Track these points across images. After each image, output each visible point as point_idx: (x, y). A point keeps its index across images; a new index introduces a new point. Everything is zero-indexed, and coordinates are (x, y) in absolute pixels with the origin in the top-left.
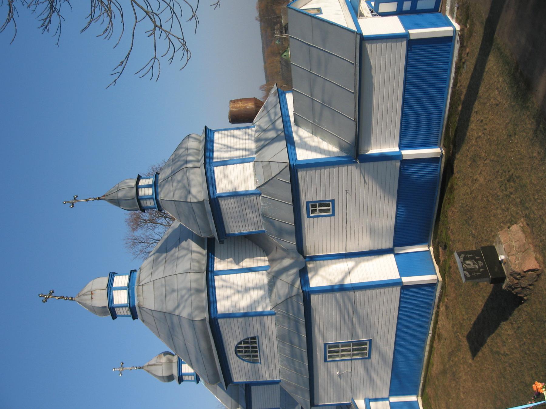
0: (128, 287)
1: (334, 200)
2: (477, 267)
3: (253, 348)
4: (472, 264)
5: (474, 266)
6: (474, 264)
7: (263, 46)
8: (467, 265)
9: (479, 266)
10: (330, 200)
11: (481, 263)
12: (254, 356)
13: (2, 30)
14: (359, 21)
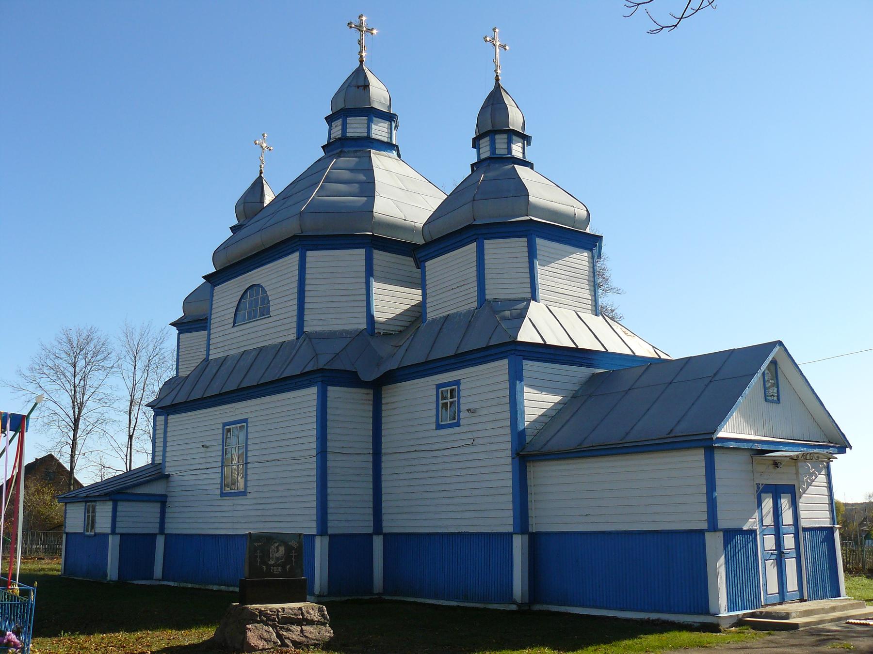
0: (480, 149)
1: (459, 426)
2: (272, 562)
3: (92, 517)
4: (277, 555)
5: (272, 558)
6: (278, 559)
7: (849, 504)
8: (277, 547)
9: (273, 565)
10: (459, 419)
11: (277, 570)
12: (24, 559)
13: (650, 32)
14: (373, 126)
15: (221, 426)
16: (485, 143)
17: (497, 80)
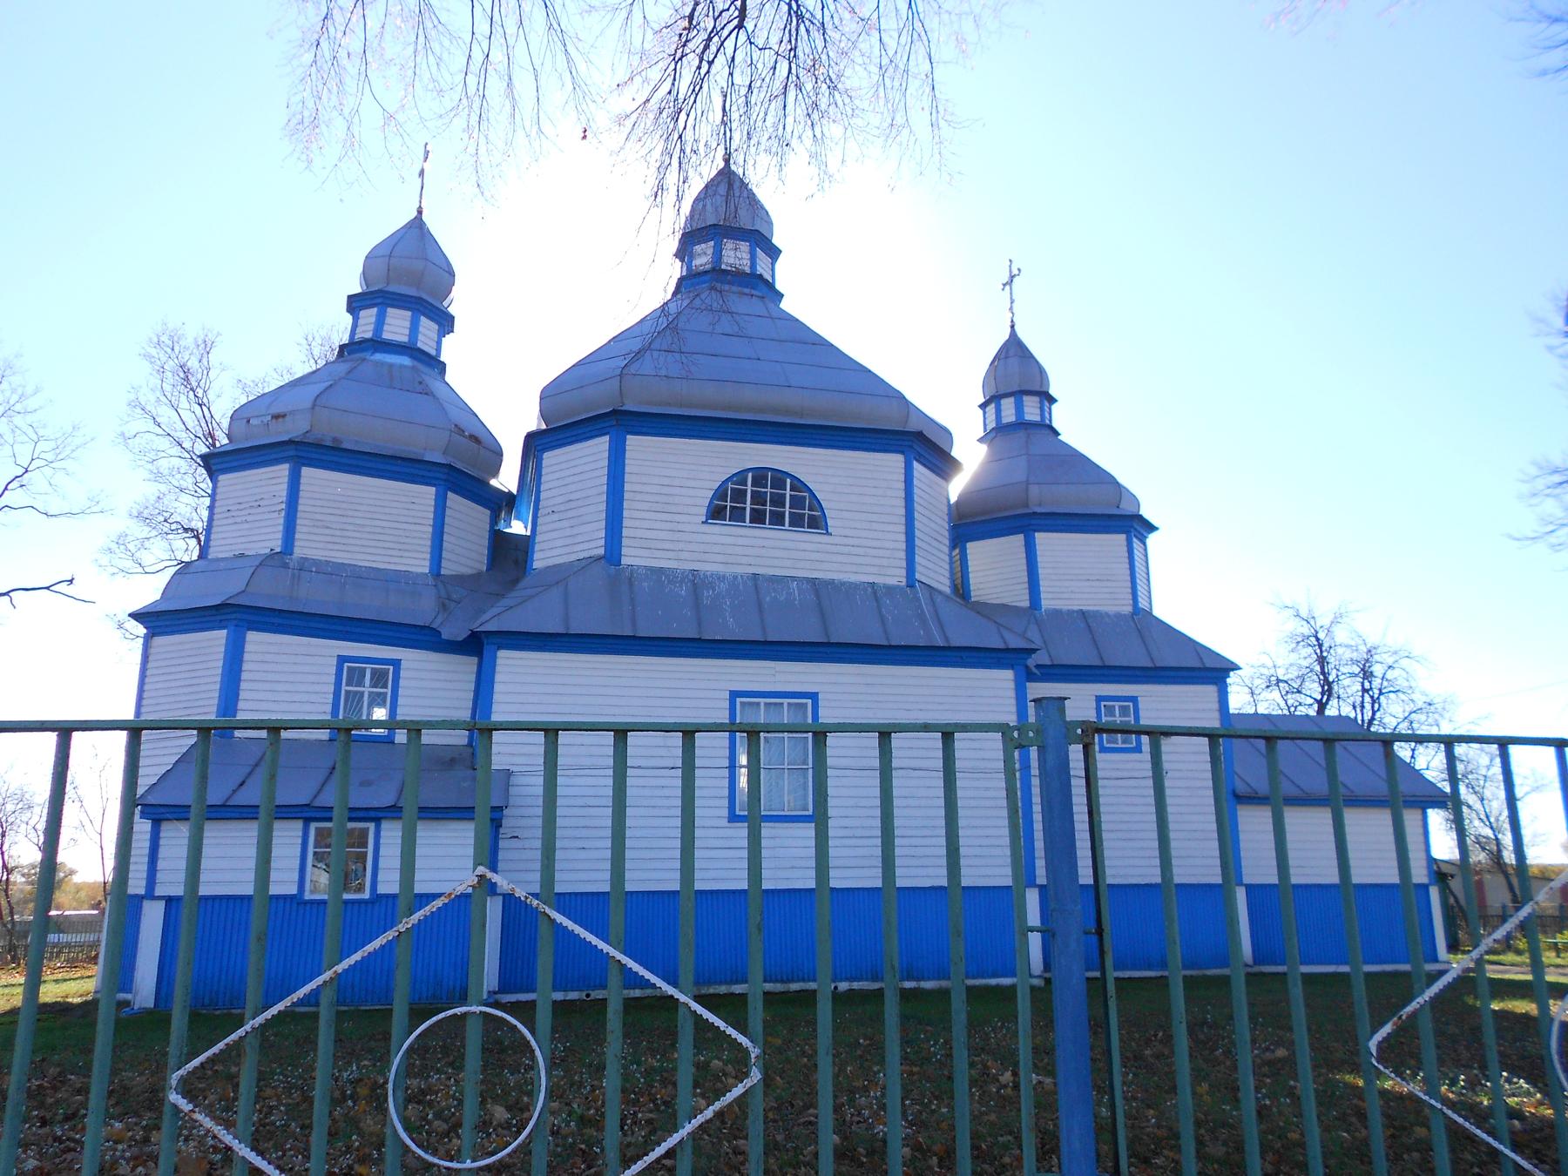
15: (727, 695)
16: (1008, 405)
17: (1012, 327)
